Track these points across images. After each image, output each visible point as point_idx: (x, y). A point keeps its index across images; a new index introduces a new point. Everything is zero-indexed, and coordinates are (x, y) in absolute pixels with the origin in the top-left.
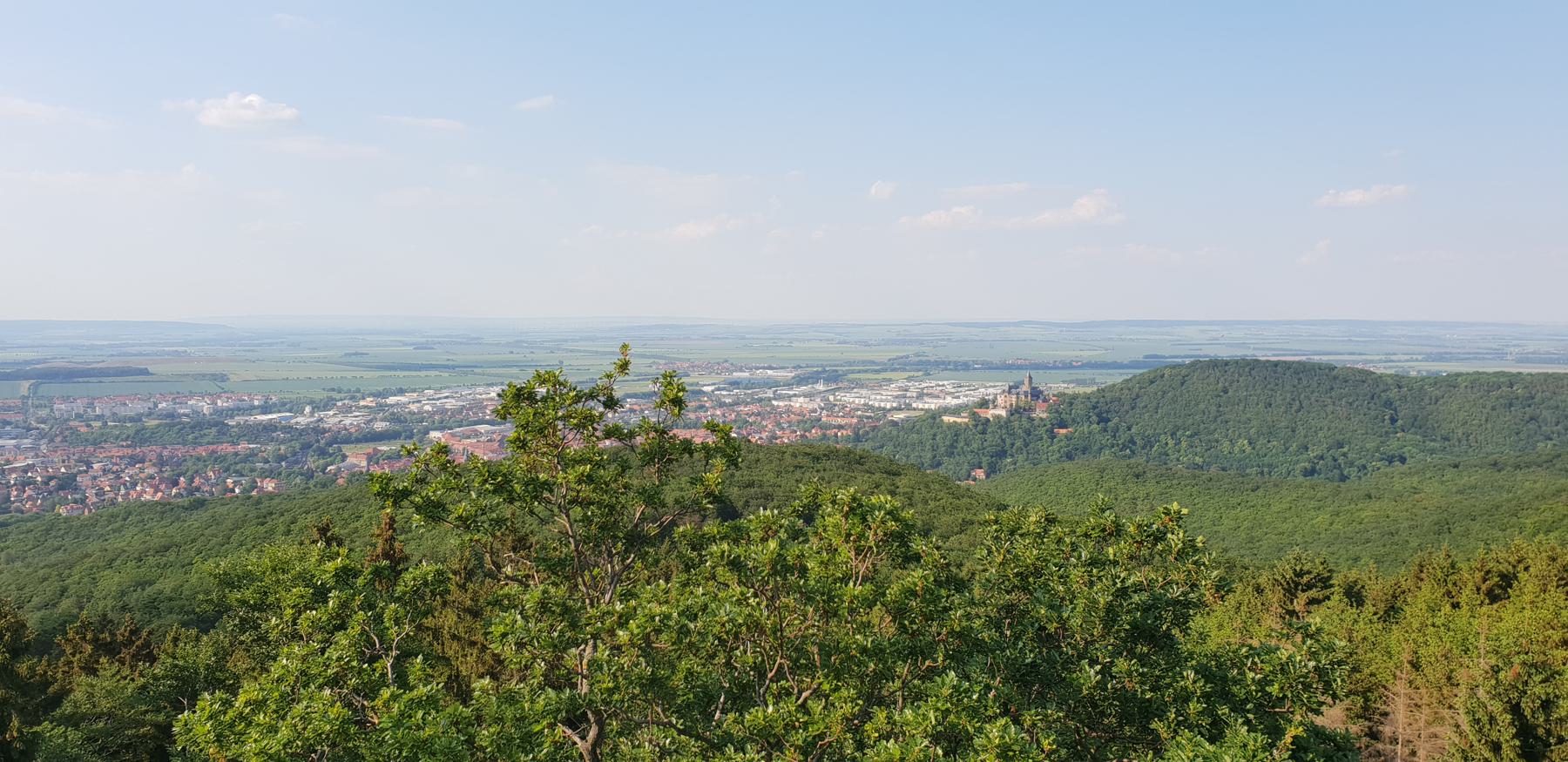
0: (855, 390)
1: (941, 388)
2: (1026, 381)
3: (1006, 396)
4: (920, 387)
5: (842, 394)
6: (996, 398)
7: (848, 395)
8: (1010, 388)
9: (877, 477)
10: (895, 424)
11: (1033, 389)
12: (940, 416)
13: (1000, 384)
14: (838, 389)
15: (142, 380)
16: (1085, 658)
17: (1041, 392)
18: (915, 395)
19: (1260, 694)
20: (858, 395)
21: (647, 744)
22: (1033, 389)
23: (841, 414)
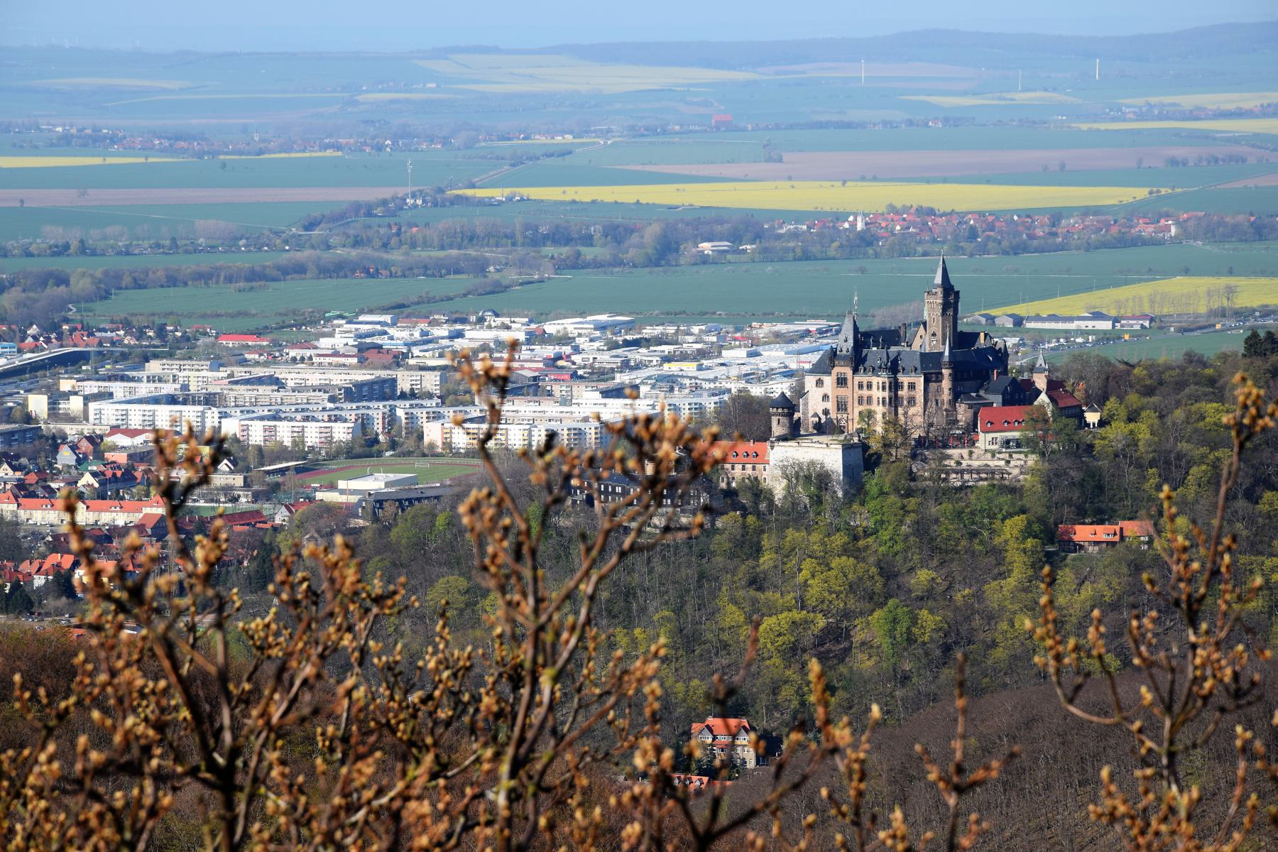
0: (154, 367)
1: (550, 351)
2: (931, 309)
3: (841, 382)
4: (459, 344)
5: (92, 387)
6: (800, 392)
7: (118, 388)
8: (862, 340)
9: (415, 620)
10: (336, 517)
11: (963, 340)
12: (527, 475)
13: (813, 325)
14: (72, 362)
15: (1231, 107)
16: (589, 777)
17: (1001, 357)
18: (431, 382)
19: (1224, 607)
20: (168, 389)
21: (696, 653)
22: (963, 340)
23: (87, 479)
